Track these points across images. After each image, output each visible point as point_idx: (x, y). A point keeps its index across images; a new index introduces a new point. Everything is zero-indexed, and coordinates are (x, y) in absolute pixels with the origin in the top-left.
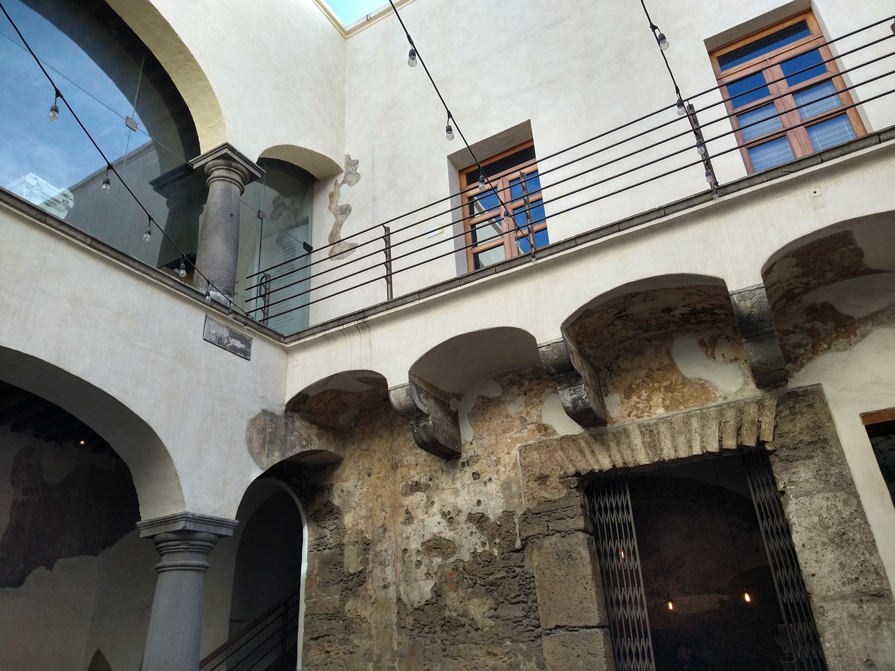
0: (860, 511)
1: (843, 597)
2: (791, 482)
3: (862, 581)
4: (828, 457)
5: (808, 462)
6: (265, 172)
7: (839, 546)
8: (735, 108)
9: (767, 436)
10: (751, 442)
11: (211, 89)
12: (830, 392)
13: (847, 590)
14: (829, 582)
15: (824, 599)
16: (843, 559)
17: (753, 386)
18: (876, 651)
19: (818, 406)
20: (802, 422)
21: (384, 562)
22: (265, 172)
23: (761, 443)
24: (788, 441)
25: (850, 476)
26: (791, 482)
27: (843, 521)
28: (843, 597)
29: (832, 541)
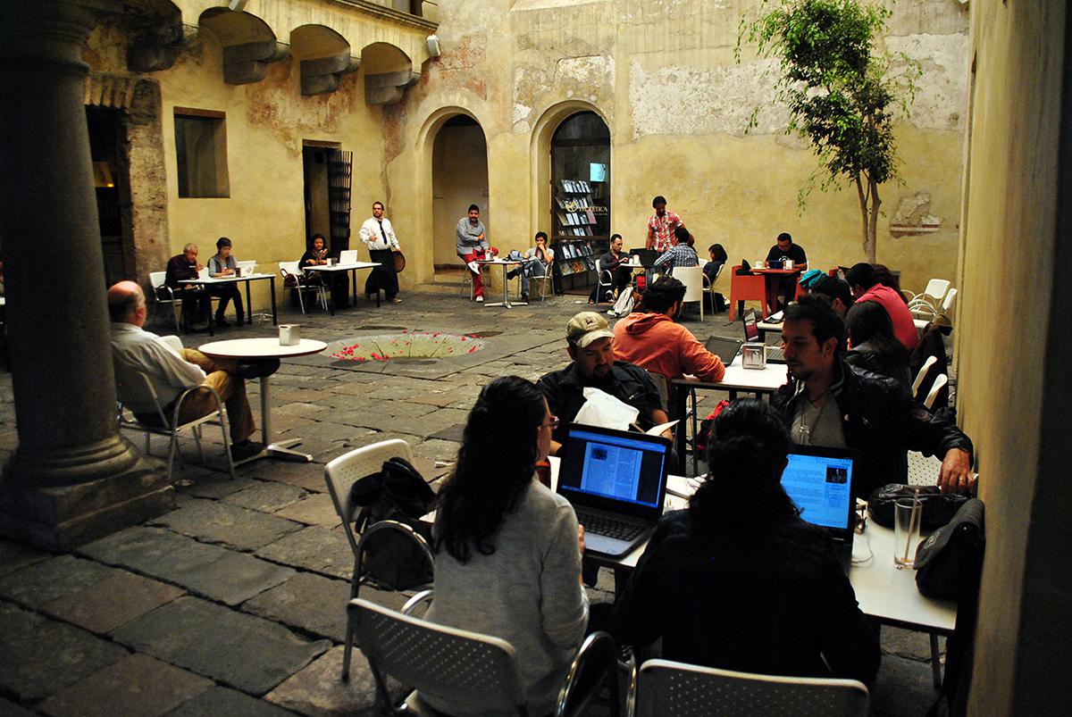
0: (162, 163)
1: (147, 207)
2: (135, 138)
3: (157, 199)
4: (154, 126)
5: (145, 127)
6: (366, 519)
7: (150, 179)
8: (180, 115)
9: (127, 105)
10: (118, 105)
11: (487, 196)
12: (163, 87)
13: (149, 203)
14: (142, 198)
15: (138, 207)
16: (151, 187)
17: (125, 68)
18: (156, 235)
19: (155, 94)
20: (146, 102)
21: (775, 423)
22: (366, 519)
23: (123, 108)
24: (137, 111)
25: (155, 62)
26: (135, 138)
27: (154, 166)
28: (147, 207)
29: (148, 176)
